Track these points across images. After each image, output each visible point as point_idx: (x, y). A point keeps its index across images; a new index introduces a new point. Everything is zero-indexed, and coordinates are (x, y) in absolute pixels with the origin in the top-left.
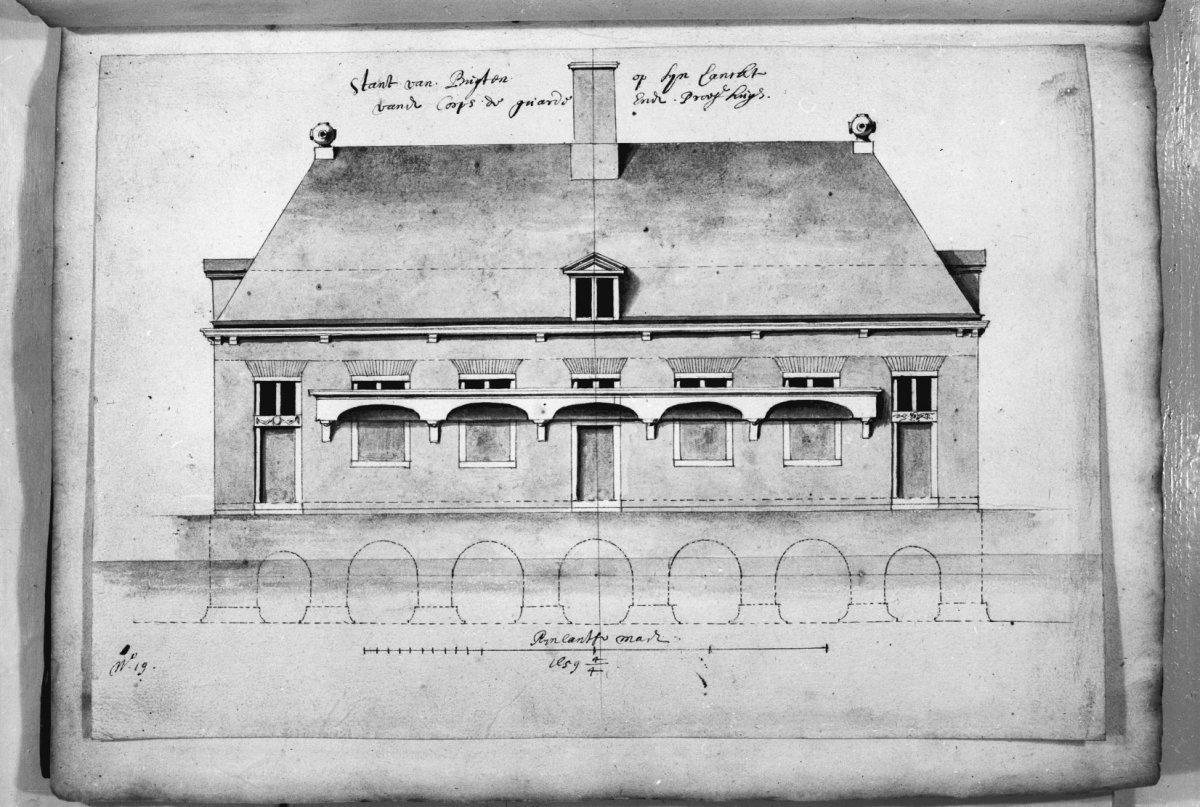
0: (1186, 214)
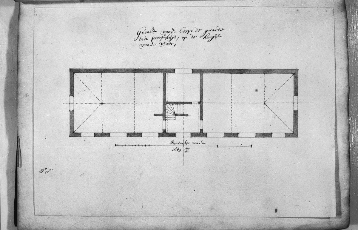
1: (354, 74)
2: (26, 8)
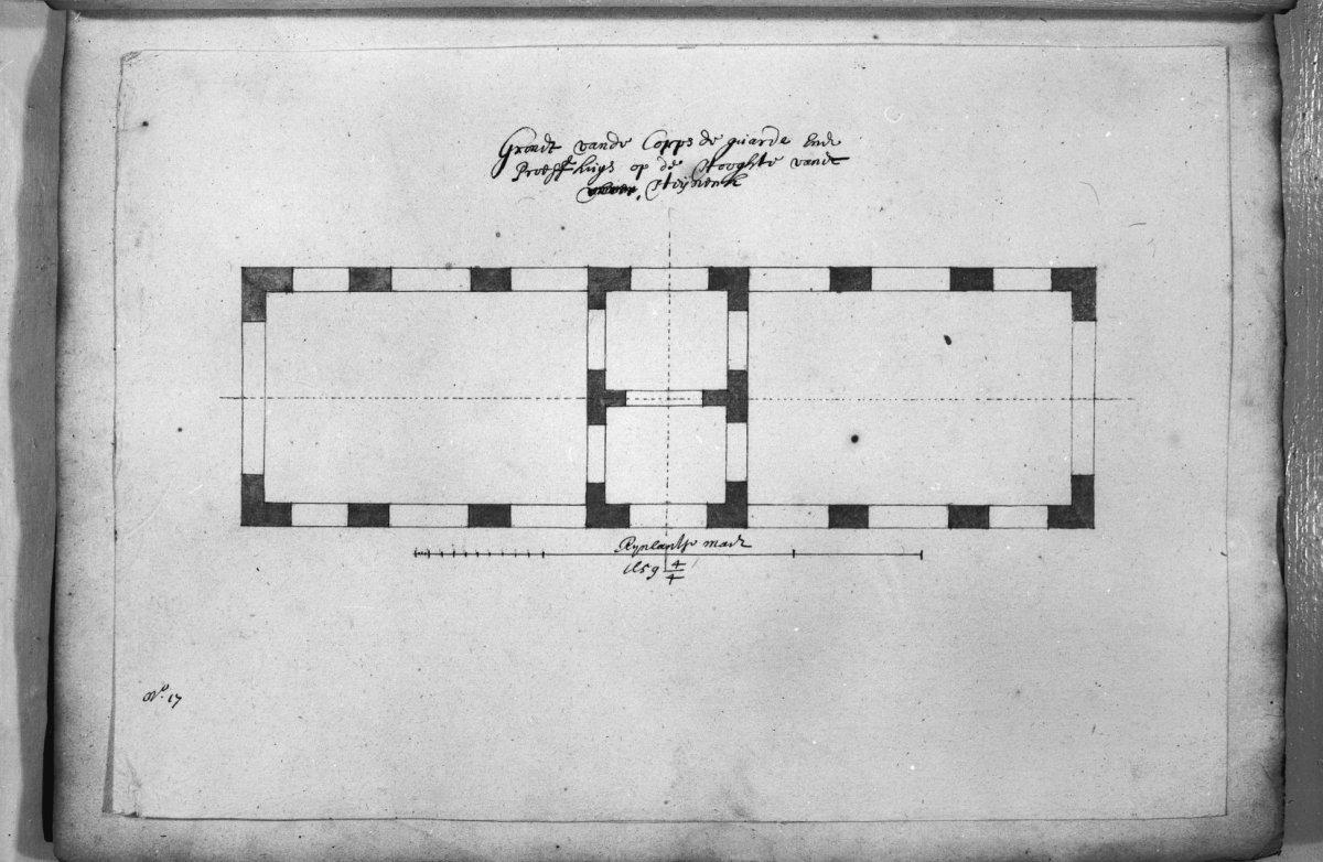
0: (1313, 231)
1: (1306, 289)
2: (98, 38)
